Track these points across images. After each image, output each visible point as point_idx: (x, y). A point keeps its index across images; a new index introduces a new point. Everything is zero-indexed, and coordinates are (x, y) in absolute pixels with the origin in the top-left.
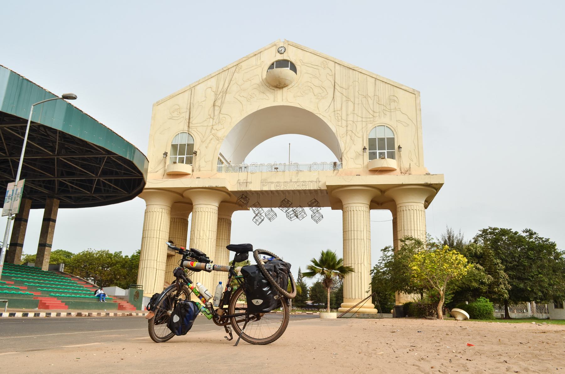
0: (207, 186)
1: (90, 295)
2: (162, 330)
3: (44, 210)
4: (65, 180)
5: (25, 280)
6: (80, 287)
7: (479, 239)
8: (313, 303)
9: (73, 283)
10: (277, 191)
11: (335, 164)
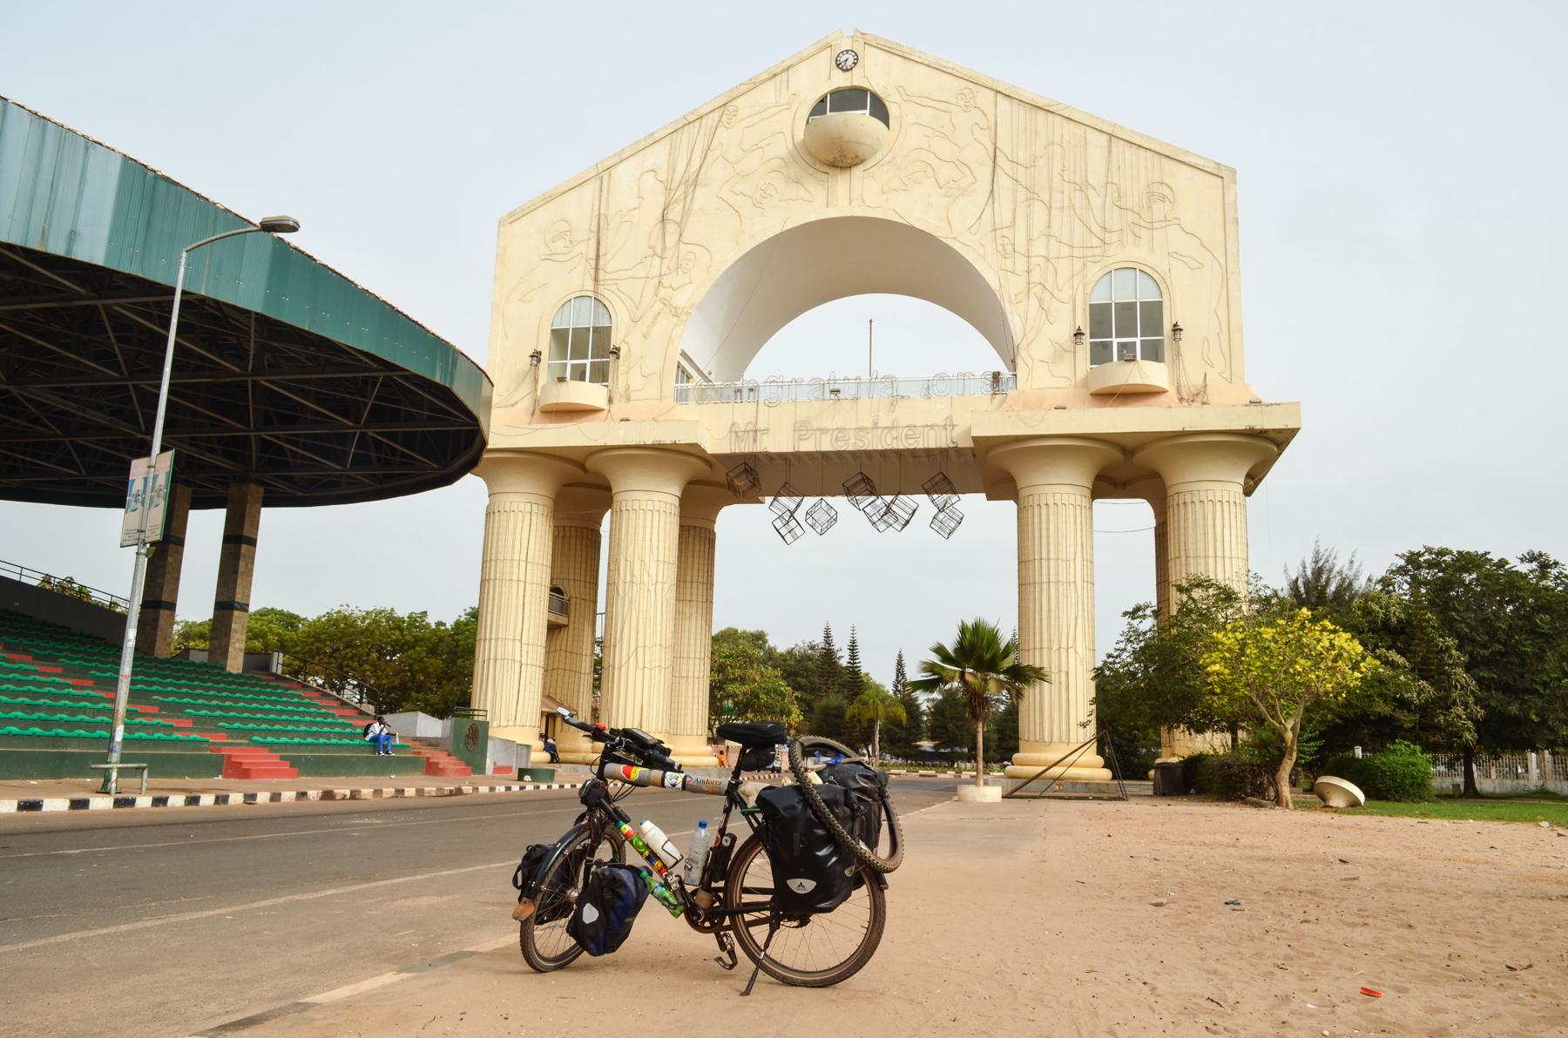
0: (649, 442)
1: (352, 736)
2: (554, 937)
3: (224, 511)
4: (277, 435)
5: (186, 700)
6: (325, 716)
7: (1399, 578)
8: (936, 747)
9: (308, 706)
10: (839, 454)
11: (996, 377)
